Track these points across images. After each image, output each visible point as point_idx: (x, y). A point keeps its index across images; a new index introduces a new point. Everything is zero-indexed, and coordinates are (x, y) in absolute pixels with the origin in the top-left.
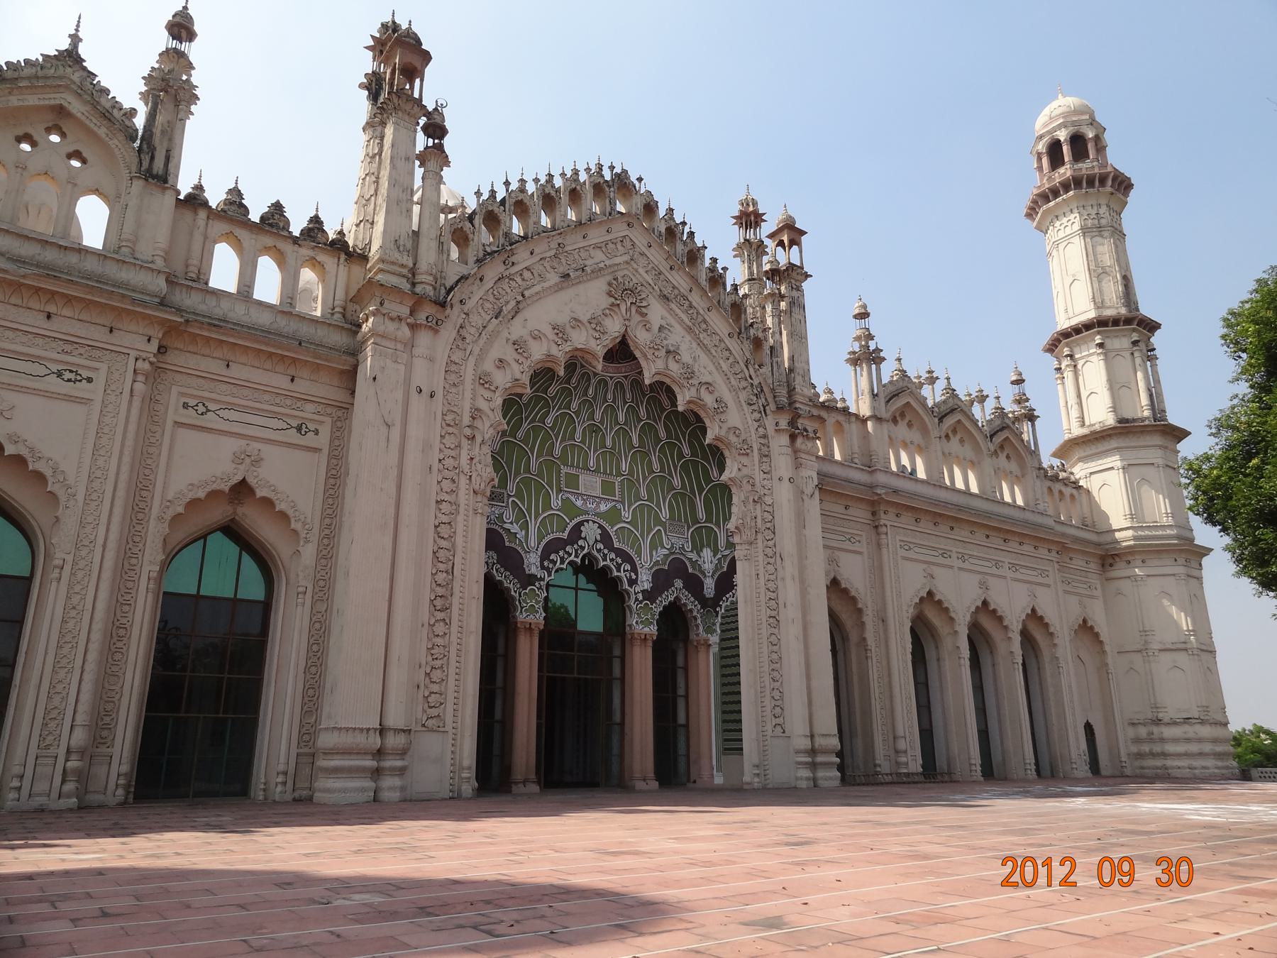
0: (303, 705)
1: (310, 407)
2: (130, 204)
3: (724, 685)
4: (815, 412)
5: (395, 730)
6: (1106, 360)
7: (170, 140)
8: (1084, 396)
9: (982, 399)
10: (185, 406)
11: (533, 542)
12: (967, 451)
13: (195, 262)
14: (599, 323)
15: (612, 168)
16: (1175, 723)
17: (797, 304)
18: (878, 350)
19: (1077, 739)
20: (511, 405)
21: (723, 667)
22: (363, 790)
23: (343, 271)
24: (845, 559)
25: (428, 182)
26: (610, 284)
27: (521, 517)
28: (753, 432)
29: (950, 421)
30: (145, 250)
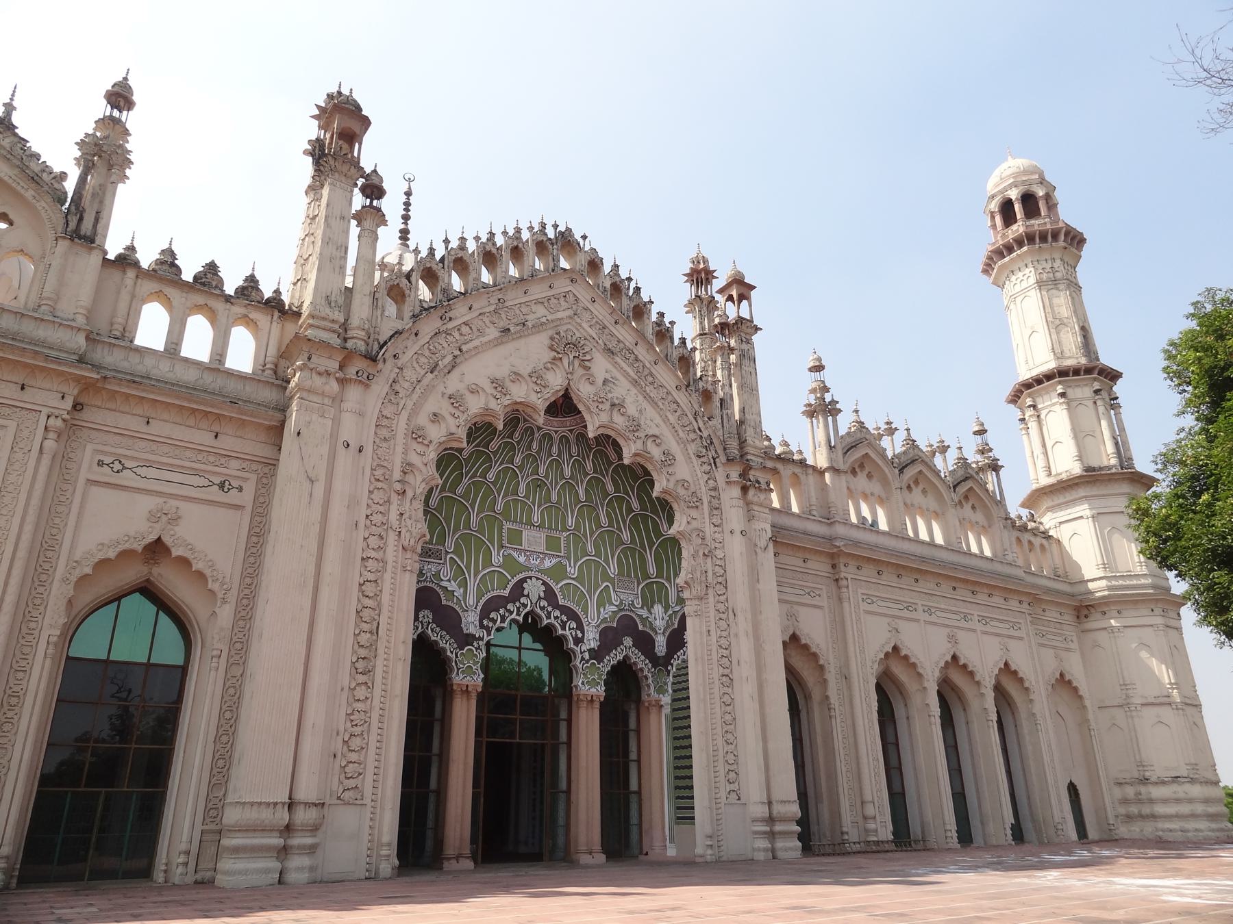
0: (211, 776)
1: (235, 464)
2: (54, 264)
3: (676, 748)
4: (770, 464)
5: (306, 804)
6: (1069, 409)
7: (101, 202)
8: (1046, 447)
9: (944, 449)
10: (100, 463)
11: (471, 600)
12: (931, 502)
13: (120, 320)
14: (540, 377)
15: (556, 226)
16: (1163, 783)
17: (747, 357)
18: (834, 402)
19: (1060, 801)
20: (448, 460)
21: (675, 729)
22: (267, 871)
23: (276, 328)
24: (803, 613)
25: (364, 240)
26: (552, 338)
27: (460, 576)
28: (703, 485)
29: (910, 472)
30: (66, 308)
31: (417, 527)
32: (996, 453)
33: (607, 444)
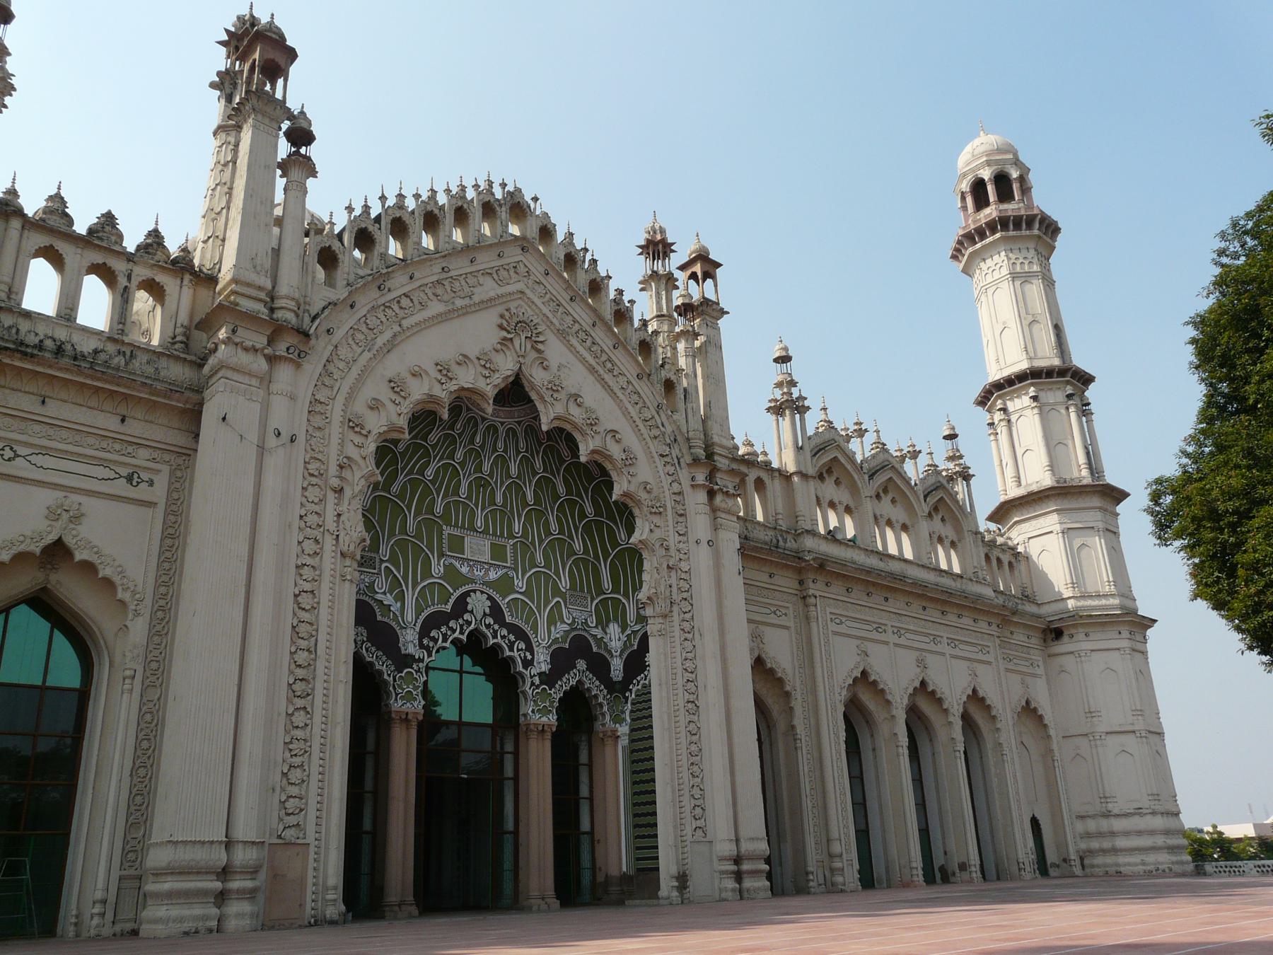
0: (129, 815)
1: (144, 453)
6: (1041, 414)
8: (1014, 456)
9: (915, 455)
11: (410, 616)
14: (489, 361)
15: (503, 185)
19: (1024, 836)
20: (386, 453)
22: (205, 918)
25: (292, 193)
27: (396, 586)
29: (881, 479)
31: (354, 531)
32: (967, 461)
33: (563, 439)
